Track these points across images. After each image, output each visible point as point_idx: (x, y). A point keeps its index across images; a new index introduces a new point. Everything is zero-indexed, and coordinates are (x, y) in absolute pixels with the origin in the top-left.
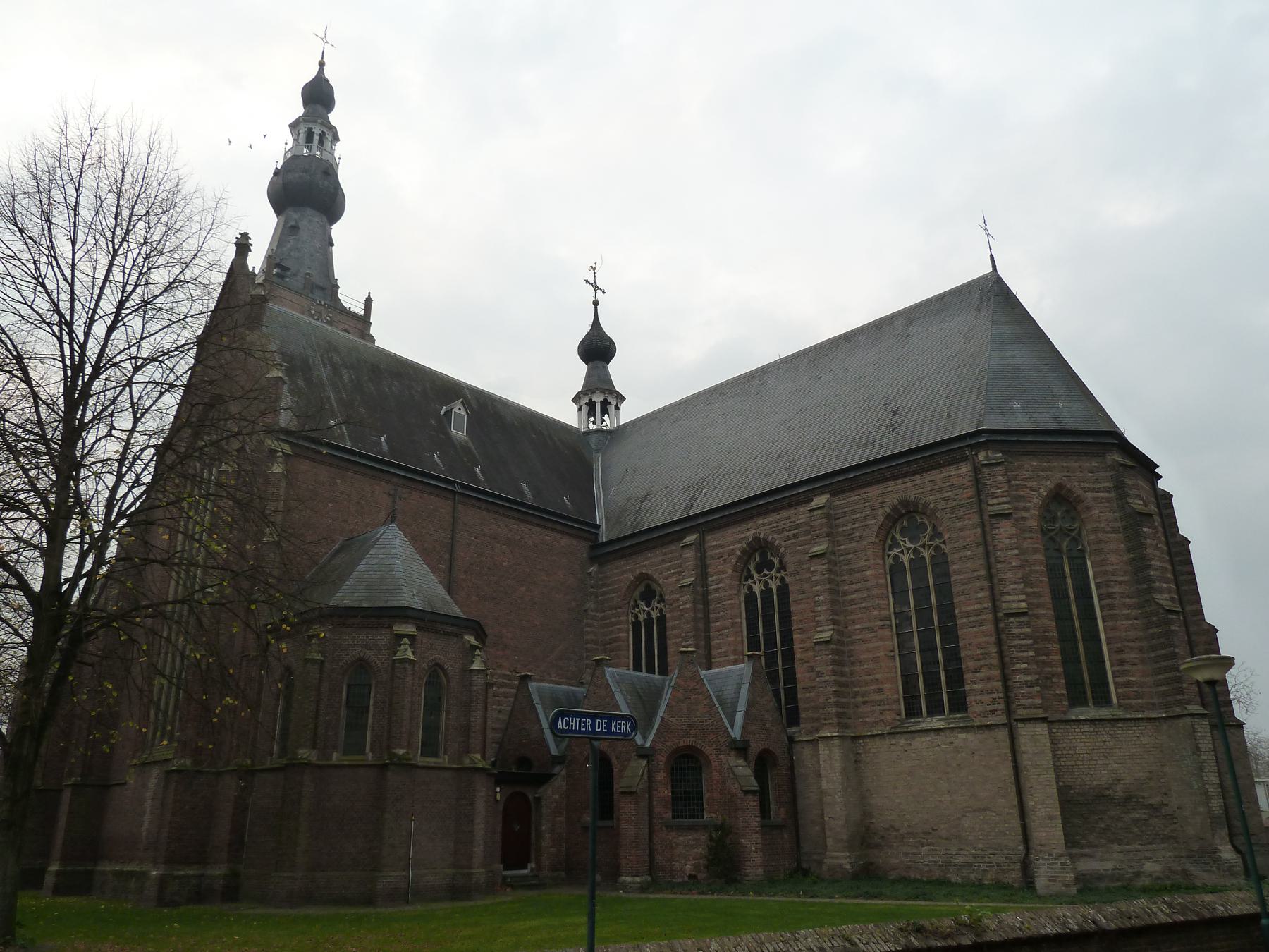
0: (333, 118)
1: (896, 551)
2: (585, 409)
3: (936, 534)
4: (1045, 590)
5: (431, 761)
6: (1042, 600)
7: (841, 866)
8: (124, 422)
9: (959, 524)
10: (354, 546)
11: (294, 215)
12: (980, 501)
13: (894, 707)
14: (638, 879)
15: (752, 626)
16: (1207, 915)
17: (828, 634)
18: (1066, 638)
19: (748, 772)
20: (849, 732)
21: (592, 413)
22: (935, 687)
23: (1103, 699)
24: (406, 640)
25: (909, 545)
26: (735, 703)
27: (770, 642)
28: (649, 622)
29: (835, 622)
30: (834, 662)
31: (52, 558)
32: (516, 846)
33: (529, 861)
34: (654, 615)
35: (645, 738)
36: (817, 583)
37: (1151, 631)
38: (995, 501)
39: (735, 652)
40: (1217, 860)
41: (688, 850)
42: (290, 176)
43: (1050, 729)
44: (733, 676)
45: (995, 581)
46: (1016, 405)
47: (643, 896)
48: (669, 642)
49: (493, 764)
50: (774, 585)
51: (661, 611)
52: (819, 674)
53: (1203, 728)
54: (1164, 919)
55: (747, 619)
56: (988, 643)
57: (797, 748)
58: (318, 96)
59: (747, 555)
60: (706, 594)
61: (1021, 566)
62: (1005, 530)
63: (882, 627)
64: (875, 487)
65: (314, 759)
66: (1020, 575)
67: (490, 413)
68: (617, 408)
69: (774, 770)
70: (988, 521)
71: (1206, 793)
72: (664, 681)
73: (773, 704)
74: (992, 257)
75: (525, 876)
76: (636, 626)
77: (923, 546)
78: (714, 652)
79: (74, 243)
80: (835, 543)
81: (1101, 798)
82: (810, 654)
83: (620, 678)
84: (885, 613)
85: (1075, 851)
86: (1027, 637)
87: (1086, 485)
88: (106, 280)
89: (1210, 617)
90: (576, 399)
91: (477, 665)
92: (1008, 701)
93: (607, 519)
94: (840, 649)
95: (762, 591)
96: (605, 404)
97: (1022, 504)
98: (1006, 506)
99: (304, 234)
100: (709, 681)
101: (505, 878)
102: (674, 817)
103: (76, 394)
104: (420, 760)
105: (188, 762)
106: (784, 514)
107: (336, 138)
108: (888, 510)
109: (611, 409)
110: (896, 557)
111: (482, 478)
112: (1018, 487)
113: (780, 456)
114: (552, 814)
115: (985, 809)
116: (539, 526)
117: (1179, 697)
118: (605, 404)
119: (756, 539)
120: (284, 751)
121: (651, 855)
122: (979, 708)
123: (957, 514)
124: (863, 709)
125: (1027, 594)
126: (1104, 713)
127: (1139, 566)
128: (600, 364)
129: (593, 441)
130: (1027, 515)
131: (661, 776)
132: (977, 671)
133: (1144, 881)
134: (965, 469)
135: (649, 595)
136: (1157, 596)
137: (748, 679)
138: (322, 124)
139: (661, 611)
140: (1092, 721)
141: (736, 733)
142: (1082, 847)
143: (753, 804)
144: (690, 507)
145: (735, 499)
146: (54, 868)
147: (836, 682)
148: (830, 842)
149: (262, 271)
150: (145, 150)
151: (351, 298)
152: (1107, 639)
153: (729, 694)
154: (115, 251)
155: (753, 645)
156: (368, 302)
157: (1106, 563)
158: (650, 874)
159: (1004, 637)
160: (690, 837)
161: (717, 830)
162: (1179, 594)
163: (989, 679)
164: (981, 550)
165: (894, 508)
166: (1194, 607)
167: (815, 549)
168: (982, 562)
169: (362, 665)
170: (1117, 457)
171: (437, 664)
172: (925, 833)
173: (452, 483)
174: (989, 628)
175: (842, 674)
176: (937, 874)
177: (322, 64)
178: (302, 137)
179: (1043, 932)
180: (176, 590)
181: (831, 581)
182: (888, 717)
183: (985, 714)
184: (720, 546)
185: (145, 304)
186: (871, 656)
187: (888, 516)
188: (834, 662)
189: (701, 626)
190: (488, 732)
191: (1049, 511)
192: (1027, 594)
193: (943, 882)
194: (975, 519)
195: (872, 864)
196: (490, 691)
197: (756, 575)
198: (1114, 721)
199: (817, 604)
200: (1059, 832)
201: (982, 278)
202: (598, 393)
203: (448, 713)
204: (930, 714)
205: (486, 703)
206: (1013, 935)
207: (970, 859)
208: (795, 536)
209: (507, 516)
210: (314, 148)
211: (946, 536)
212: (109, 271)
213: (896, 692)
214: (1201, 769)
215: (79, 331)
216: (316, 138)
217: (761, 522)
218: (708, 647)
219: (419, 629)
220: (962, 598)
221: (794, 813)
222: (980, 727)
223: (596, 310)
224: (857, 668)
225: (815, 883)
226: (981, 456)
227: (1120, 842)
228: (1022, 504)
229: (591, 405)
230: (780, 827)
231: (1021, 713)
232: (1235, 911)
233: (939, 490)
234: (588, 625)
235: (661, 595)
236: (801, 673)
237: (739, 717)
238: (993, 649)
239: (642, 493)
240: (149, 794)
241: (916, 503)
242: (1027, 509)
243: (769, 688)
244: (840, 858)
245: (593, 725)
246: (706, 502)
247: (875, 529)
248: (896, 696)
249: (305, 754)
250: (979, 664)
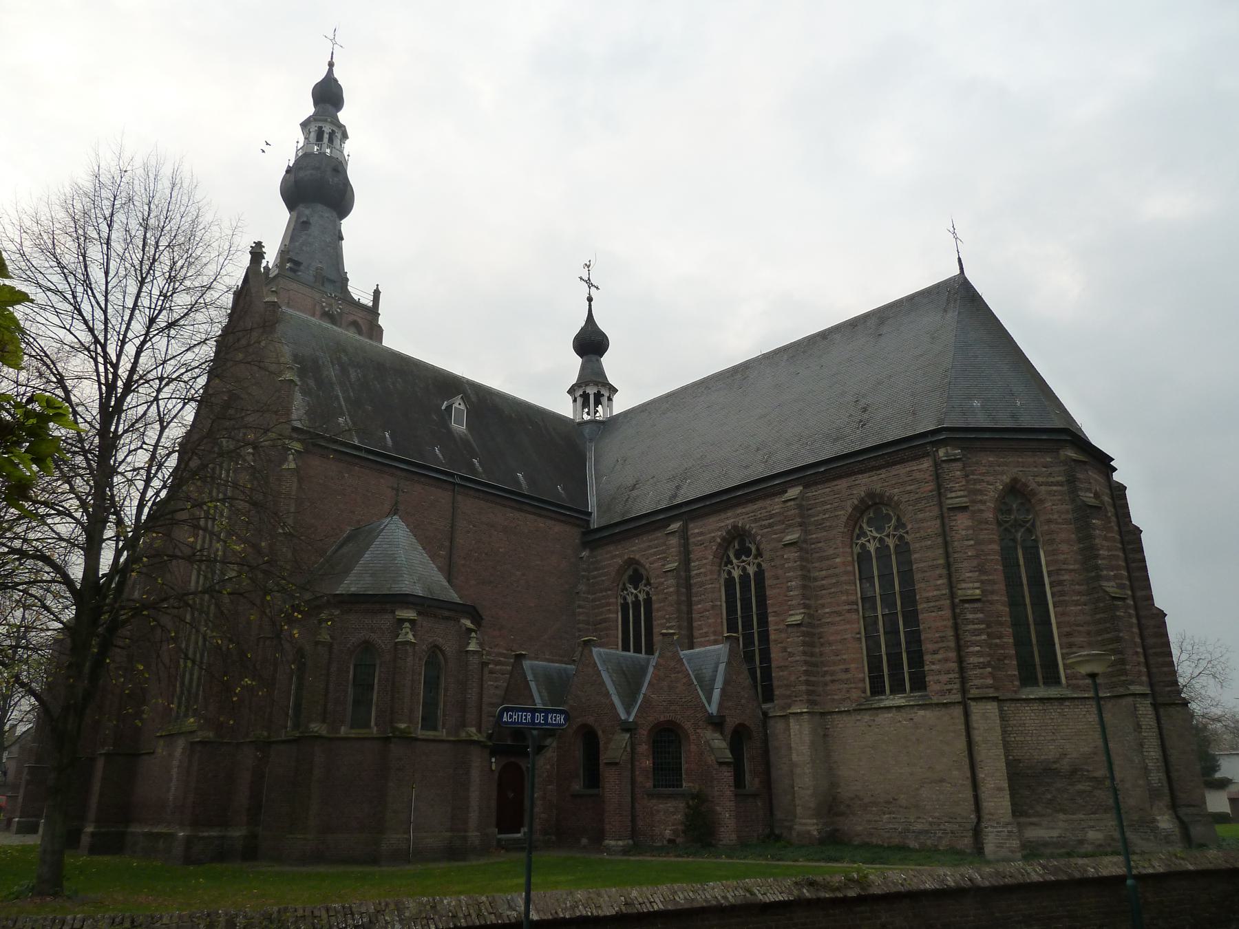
0: (342, 116)
1: (863, 540)
2: (580, 401)
3: (900, 525)
4: (999, 577)
5: (430, 734)
6: (996, 587)
7: (809, 832)
8: (152, 435)
9: (921, 516)
10: (362, 536)
11: (301, 208)
12: (940, 494)
13: (860, 685)
14: (620, 843)
15: (731, 609)
16: (1077, 875)
17: (799, 617)
18: (1018, 623)
19: (724, 745)
20: (818, 709)
21: (586, 404)
22: (897, 668)
23: (1052, 678)
24: (407, 624)
25: (875, 534)
26: (713, 680)
27: (748, 624)
28: (636, 604)
29: (806, 606)
30: (804, 644)
31: (92, 551)
32: (510, 813)
33: (522, 825)
34: (641, 597)
35: (629, 713)
36: (790, 569)
37: (1098, 616)
38: (953, 495)
39: (715, 633)
40: (1154, 830)
41: (668, 816)
42: (301, 174)
43: (1001, 710)
44: (712, 655)
45: (953, 569)
46: (976, 403)
47: (625, 858)
48: (655, 623)
49: (490, 737)
50: (751, 570)
51: (648, 594)
52: (791, 655)
53: (1145, 709)
54: (1035, 878)
55: (727, 602)
56: (945, 627)
57: (771, 722)
58: (328, 95)
59: (727, 542)
60: (688, 578)
61: (977, 556)
62: (962, 522)
63: (849, 611)
64: (844, 480)
65: (324, 733)
66: (975, 563)
67: (490, 408)
68: (610, 399)
69: (749, 744)
70: (946, 514)
71: (1146, 768)
72: (648, 661)
73: (748, 682)
74: (959, 259)
75: (519, 839)
76: (625, 607)
77: (888, 536)
78: (696, 633)
79: (107, 273)
80: (806, 532)
81: (1049, 771)
82: (783, 635)
83: (606, 657)
84: (853, 598)
85: (1022, 820)
86: (981, 622)
87: (1040, 479)
88: (135, 304)
89: (1159, 602)
90: (571, 391)
91: (472, 647)
92: (963, 680)
93: (599, 506)
94: (811, 631)
95: (740, 576)
97: (979, 498)
98: (965, 499)
99: (315, 230)
100: (689, 661)
101: (499, 841)
102: (654, 786)
103: (110, 409)
104: (420, 733)
105: (211, 735)
106: (760, 504)
107: (345, 136)
108: (856, 502)
110: (863, 546)
111: (480, 469)
112: (976, 482)
113: (758, 449)
114: (540, 787)
115: (942, 780)
116: (534, 514)
117: (1123, 678)
119: (735, 527)
120: (296, 726)
121: (633, 820)
122: (937, 687)
123: (919, 506)
124: (831, 687)
125: (982, 582)
126: (1053, 692)
127: (1089, 554)
128: (594, 358)
129: (587, 430)
130: (983, 507)
131: (643, 748)
132: (935, 652)
133: (1088, 848)
134: (926, 464)
135: (637, 579)
136: (1104, 584)
137: (724, 658)
138: (332, 123)
139: (648, 594)
140: (1041, 700)
141: (713, 709)
142: (1029, 817)
143: (727, 775)
144: (675, 496)
145: (716, 490)
146: (90, 829)
147: (806, 662)
148: (799, 810)
149: (276, 265)
150: (168, 185)
151: (360, 290)
152: (1058, 623)
153: (708, 673)
154: (143, 279)
155: (732, 627)
156: (377, 294)
157: (1058, 553)
158: (632, 838)
159: (959, 621)
160: (670, 805)
161: (693, 799)
162: (1130, 581)
163: (946, 660)
164: (940, 540)
165: (862, 501)
166: (1144, 593)
167: (788, 538)
168: (941, 551)
169: (367, 647)
170: (1071, 453)
171: (436, 646)
172: (888, 802)
173: (452, 475)
174: (947, 613)
175: (812, 655)
176: (896, 841)
177: (331, 65)
178: (313, 136)
179: (922, 887)
180: (197, 582)
181: (802, 568)
182: (855, 694)
183: (943, 693)
184: (701, 534)
185: (171, 325)
186: (839, 637)
187: (855, 508)
188: (804, 644)
189: (684, 608)
190: (484, 707)
191: (1005, 503)
192: (982, 582)
193: (902, 848)
194: (936, 512)
195: (837, 830)
196: (486, 670)
197: (735, 561)
198: (1061, 700)
199: (789, 589)
200: (1006, 803)
201: (950, 279)
202: (591, 386)
203: (446, 690)
204: (893, 692)
205: (482, 679)
206: (894, 890)
207: (926, 827)
208: (770, 526)
209: (505, 506)
211: (909, 527)
212: (138, 296)
213: (861, 672)
214: (1142, 745)
215: (112, 350)
216: (326, 136)
217: (739, 511)
218: (690, 628)
219: (419, 614)
220: (922, 585)
221: (768, 783)
222: (937, 705)
224: (827, 649)
225: (785, 847)
226: (941, 452)
227: (1064, 811)
228: (979, 498)
229: (585, 397)
230: (755, 796)
231: (974, 692)
232: (1105, 873)
233: (903, 484)
234: (579, 607)
235: (648, 579)
236: (776, 654)
237: (716, 694)
238: (950, 633)
239: (631, 482)
240: (176, 763)
241: (881, 496)
242: (983, 502)
243: (745, 667)
244: (808, 825)
245: (533, 718)
246: (689, 492)
247: (844, 519)
248: (861, 675)
249: (316, 727)
250: (936, 646)
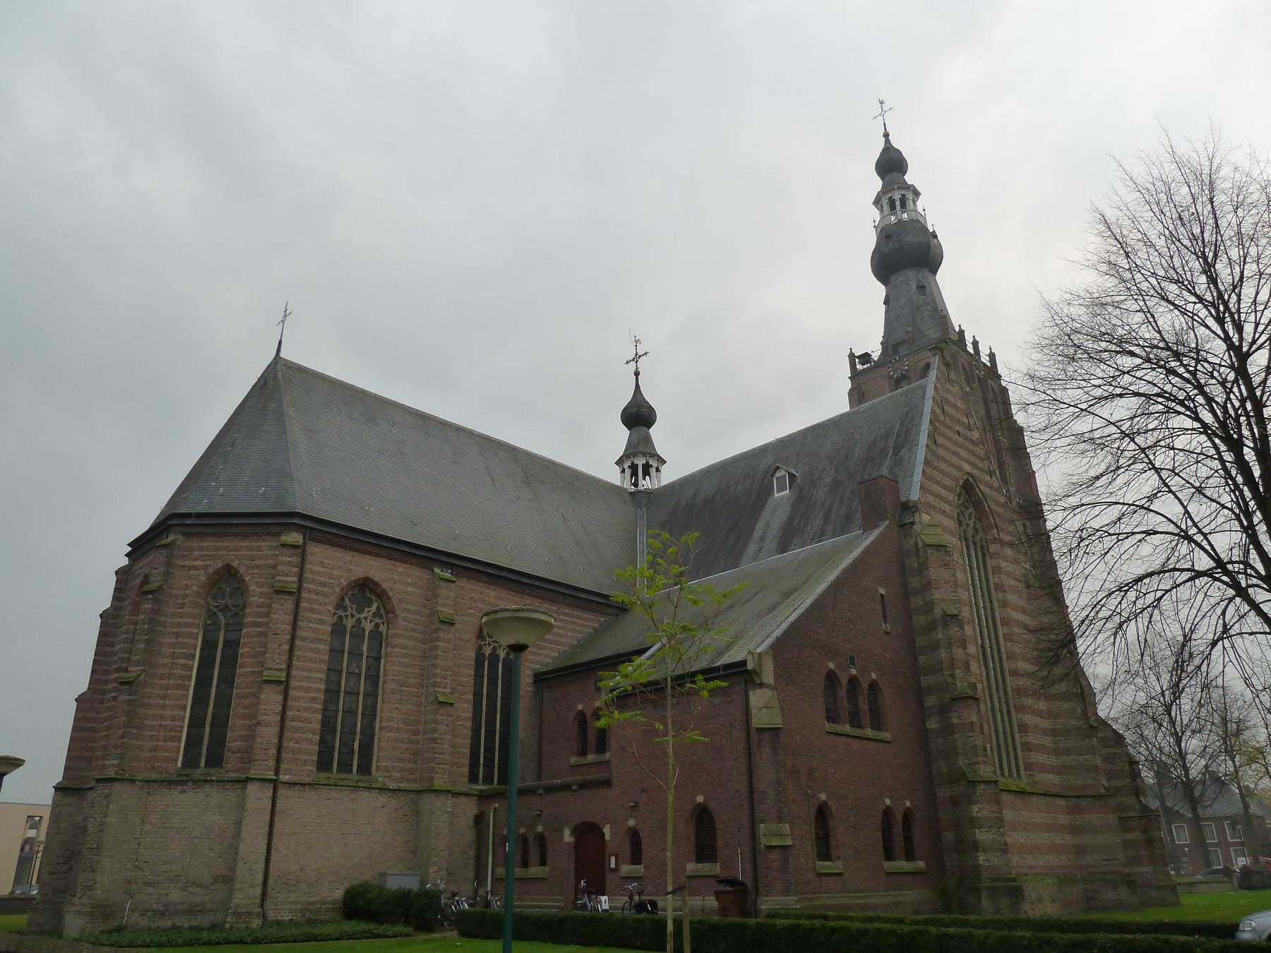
0: (909, 178)
2: (628, 472)
28: (358, 634)
58: (891, 165)
68: (658, 470)
96: (647, 467)
107: (917, 194)
109: (653, 471)
118: (647, 467)
152: (181, 732)
177: (886, 135)
178: (886, 208)
202: (640, 456)
210: (899, 213)
216: (898, 203)
229: (634, 468)
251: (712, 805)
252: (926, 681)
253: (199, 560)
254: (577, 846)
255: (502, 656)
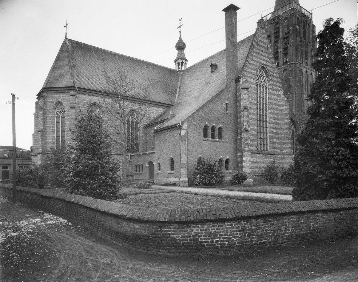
2: (177, 65)
74: (66, 33)
96: (182, 63)
109: (184, 64)
118: (182, 63)
202: (181, 60)
223: (180, 34)
229: (178, 63)
251: (173, 158)
252: (239, 126)
253: (52, 99)
254: (149, 167)
255: (135, 122)
